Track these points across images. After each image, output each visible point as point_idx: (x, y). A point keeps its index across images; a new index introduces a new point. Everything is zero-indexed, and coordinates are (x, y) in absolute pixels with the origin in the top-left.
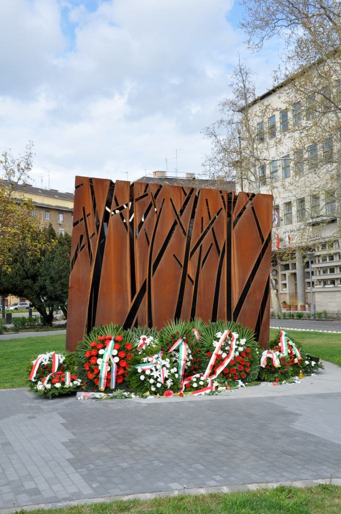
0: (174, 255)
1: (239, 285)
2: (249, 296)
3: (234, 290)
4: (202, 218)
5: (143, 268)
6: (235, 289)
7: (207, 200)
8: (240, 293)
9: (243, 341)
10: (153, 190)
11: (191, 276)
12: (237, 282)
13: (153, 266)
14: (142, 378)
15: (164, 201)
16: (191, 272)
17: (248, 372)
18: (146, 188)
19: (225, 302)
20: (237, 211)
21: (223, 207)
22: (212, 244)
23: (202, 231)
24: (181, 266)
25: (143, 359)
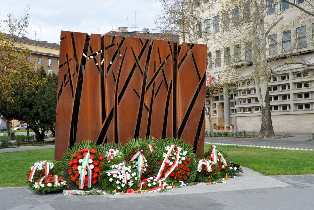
0: (134, 90)
2: (189, 119)
3: (179, 116)
4: (155, 62)
8: (182, 117)
10: (118, 41)
11: (146, 105)
16: (147, 102)
19: (172, 124)
21: (171, 54)
22: (162, 81)
24: (139, 97)
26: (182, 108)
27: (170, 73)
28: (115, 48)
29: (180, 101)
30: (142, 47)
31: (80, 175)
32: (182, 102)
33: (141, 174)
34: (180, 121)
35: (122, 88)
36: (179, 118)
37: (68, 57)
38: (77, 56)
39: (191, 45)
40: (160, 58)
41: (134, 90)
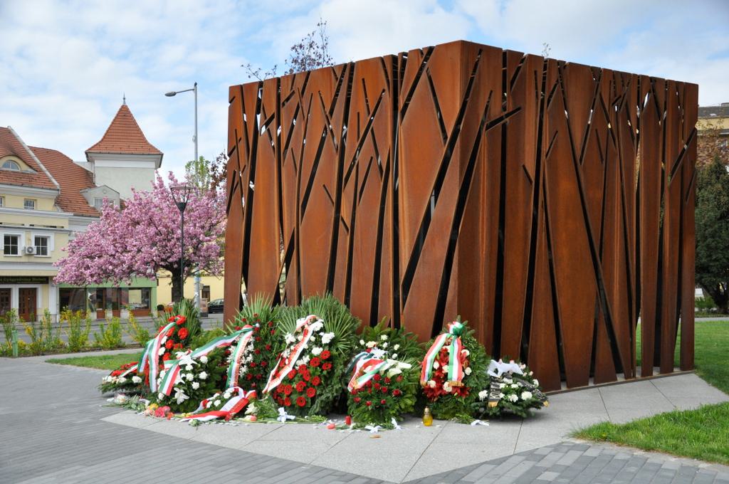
0: (324, 186)
1: (410, 230)
2: (425, 249)
3: (403, 241)
4: (358, 113)
5: (291, 212)
6: (404, 239)
7: (363, 80)
8: (411, 245)
9: (327, 338)
10: (299, 83)
11: (345, 220)
12: (407, 224)
13: (302, 206)
14: (203, 375)
15: (490, 94)
16: (345, 213)
17: (496, 411)
18: (279, 86)
19: (389, 264)
20: (407, 83)
21: (386, 88)
22: (372, 158)
23: (445, 138)
24: (333, 203)
25: (521, 373)
26: (410, 223)
27: (386, 135)
28: (295, 100)
29: (405, 203)
30: (335, 84)
31: (150, 367)
32: (409, 206)
33: (236, 377)
34: (405, 255)
35: (452, 274)
36: (403, 248)
37: (245, 145)
38: (273, 153)
39: (425, 53)
40: (368, 105)
41: (324, 186)
